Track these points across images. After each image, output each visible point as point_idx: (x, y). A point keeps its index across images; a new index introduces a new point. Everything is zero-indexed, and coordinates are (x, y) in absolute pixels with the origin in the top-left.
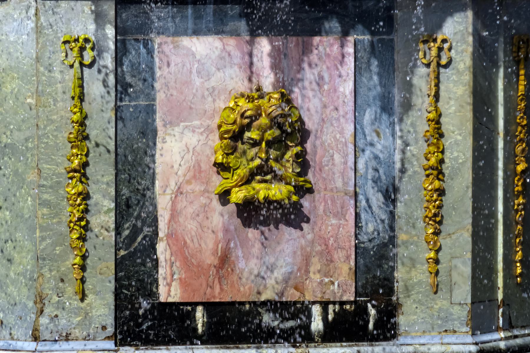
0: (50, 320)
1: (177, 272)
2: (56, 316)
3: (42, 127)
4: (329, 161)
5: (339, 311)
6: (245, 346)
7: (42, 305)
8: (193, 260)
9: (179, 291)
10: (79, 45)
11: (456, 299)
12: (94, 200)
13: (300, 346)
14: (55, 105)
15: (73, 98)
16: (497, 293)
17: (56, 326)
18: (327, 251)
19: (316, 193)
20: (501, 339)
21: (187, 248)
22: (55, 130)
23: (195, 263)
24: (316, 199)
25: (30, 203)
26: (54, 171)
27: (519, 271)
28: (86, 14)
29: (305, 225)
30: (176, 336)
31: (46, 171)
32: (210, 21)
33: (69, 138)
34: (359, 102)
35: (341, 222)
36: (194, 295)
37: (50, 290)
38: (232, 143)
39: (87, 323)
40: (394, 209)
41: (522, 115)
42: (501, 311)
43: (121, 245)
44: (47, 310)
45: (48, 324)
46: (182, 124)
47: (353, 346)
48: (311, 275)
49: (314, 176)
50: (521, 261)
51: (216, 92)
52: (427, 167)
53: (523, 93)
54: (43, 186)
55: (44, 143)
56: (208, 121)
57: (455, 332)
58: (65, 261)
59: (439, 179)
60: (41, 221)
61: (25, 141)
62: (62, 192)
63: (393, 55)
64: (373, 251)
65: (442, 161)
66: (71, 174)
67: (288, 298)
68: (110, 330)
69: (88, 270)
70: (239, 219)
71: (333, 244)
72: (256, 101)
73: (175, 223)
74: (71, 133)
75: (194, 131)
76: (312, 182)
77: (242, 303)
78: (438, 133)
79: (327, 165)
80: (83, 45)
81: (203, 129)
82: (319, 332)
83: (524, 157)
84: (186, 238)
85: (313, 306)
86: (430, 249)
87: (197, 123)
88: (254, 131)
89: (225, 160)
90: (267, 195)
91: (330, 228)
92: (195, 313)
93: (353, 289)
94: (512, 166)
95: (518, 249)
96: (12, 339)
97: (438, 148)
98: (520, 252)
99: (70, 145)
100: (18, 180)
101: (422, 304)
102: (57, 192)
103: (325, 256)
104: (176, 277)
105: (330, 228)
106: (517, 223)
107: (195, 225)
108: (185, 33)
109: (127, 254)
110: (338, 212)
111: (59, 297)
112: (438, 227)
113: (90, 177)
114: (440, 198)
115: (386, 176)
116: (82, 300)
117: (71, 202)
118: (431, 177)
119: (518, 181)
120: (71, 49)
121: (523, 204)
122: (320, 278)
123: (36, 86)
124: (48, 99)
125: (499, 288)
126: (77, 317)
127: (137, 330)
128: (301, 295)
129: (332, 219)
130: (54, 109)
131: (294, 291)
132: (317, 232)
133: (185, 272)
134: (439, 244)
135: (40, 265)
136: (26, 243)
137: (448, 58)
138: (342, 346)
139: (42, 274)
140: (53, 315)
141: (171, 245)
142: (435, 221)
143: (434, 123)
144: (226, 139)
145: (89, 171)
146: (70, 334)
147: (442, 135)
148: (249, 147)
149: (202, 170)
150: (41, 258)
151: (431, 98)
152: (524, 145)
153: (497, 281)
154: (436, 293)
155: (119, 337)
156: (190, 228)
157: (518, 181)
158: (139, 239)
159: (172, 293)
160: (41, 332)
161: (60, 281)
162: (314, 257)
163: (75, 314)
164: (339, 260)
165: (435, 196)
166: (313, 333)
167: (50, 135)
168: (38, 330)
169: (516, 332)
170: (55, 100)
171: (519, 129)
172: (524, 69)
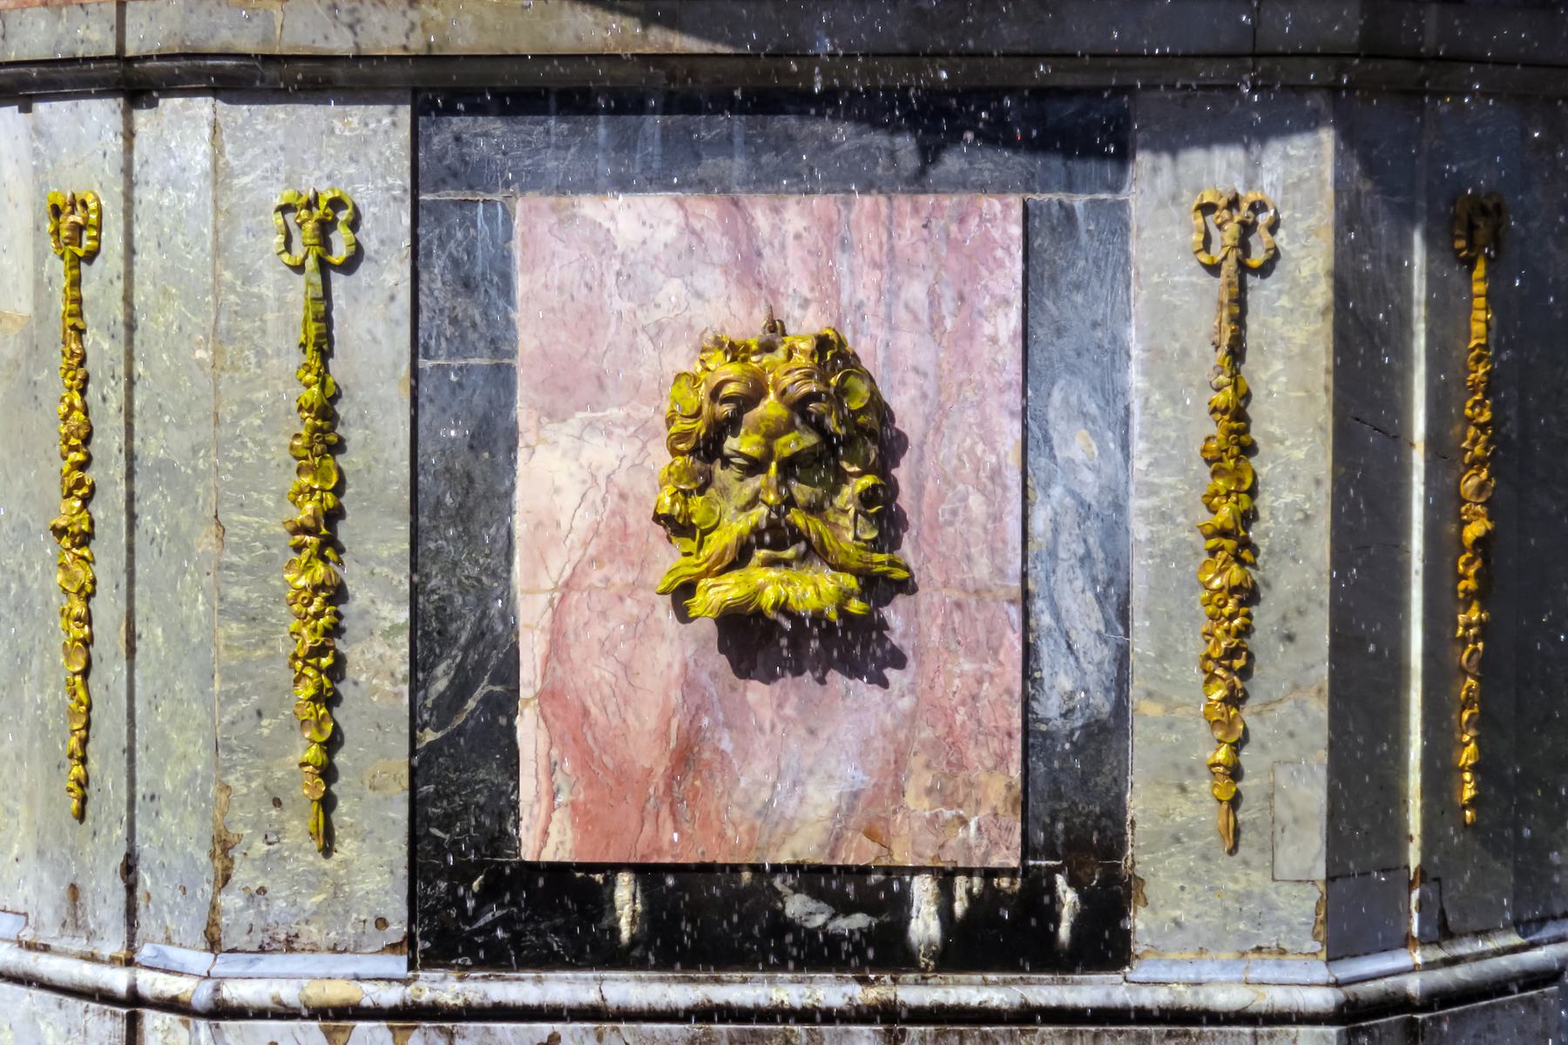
0: (248, 900)
1: (565, 788)
2: (262, 890)
3: (228, 419)
4: (954, 513)
5: (982, 895)
6: (737, 976)
7: (227, 862)
8: (606, 759)
9: (569, 834)
10: (317, 214)
11: (1284, 869)
12: (356, 603)
13: (877, 979)
14: (259, 365)
15: (303, 346)
16: (1406, 849)
17: (259, 913)
18: (950, 740)
19: (921, 591)
20: (1413, 969)
21: (590, 726)
22: (259, 426)
23: (611, 766)
24: (923, 608)
25: (201, 608)
26: (258, 530)
27: (1468, 793)
28: (339, 137)
29: (891, 674)
30: (564, 948)
31: (237, 531)
32: (652, 156)
33: (292, 447)
34: (1037, 358)
35: (986, 667)
36: (608, 845)
37: (245, 825)
38: (698, 465)
39: (340, 910)
40: (1127, 634)
41: (1478, 397)
42: (1415, 895)
43: (426, 717)
44: (241, 874)
45: (242, 910)
46: (580, 415)
47: (1014, 982)
48: (910, 800)
49: (917, 548)
50: (1475, 769)
51: (668, 333)
52: (1209, 529)
53: (1483, 341)
54: (229, 567)
55: (233, 460)
56: (645, 408)
57: (1283, 952)
58: (284, 754)
59: (1241, 562)
60: (224, 654)
61: (191, 454)
62: (278, 583)
63: (1125, 243)
64: (1072, 743)
65: (1248, 518)
66: (298, 538)
67: (847, 857)
68: (397, 929)
69: (342, 779)
70: (723, 657)
71: (964, 722)
72: (754, 359)
73: (560, 661)
74: (297, 436)
75: (609, 434)
76: (913, 566)
77: (736, 869)
78: (1237, 444)
79: (951, 524)
80: (327, 215)
81: (632, 429)
82: (930, 944)
83: (1483, 504)
84: (589, 703)
85: (916, 879)
86: (1220, 741)
87: (615, 413)
88: (746, 433)
89: (678, 507)
90: (783, 599)
91: (957, 682)
92: (613, 892)
93: (1017, 838)
94: (1452, 528)
95: (1466, 738)
96: (169, 941)
97: (1240, 481)
98: (1472, 745)
99: (296, 464)
100: (179, 550)
101: (1197, 880)
102: (265, 581)
103: (943, 754)
104: (561, 799)
105: (957, 682)
106: (1464, 673)
107: (610, 669)
108: (590, 186)
109: (442, 738)
110: (978, 641)
111: (270, 844)
112: (1239, 685)
113: (346, 547)
114: (1244, 610)
115: (1104, 551)
116: (327, 851)
117: (296, 607)
118: (1222, 555)
119: (1468, 564)
120: (1220, 227)
121: (1480, 623)
122: (931, 809)
123: (213, 317)
124: (242, 351)
125: (1411, 838)
126: (314, 895)
127: (467, 928)
128: (880, 851)
129: (962, 660)
130: (259, 376)
131: (865, 839)
132: (923, 692)
133: (585, 788)
134: (1241, 727)
135: (220, 762)
136: (195, 706)
137: (1268, 250)
138: (986, 983)
139: (228, 787)
140: (254, 888)
141: (551, 719)
142: (1229, 669)
143: (1227, 417)
144: (682, 453)
145: (344, 532)
146: (297, 936)
147: (1249, 450)
148: (738, 475)
149: (630, 531)
150: (224, 746)
151: (1222, 352)
152: (1484, 475)
153: (1406, 822)
154: (1233, 851)
155: (422, 945)
156: (597, 677)
157: (1468, 564)
158: (471, 704)
159: (554, 838)
160: (224, 929)
161: (271, 805)
162: (915, 754)
163: (310, 886)
164: (982, 763)
165: (1231, 607)
166: (915, 949)
167: (247, 439)
168: (217, 925)
169: (1465, 948)
170: (260, 353)
171: (1472, 431)
172: (1484, 279)
